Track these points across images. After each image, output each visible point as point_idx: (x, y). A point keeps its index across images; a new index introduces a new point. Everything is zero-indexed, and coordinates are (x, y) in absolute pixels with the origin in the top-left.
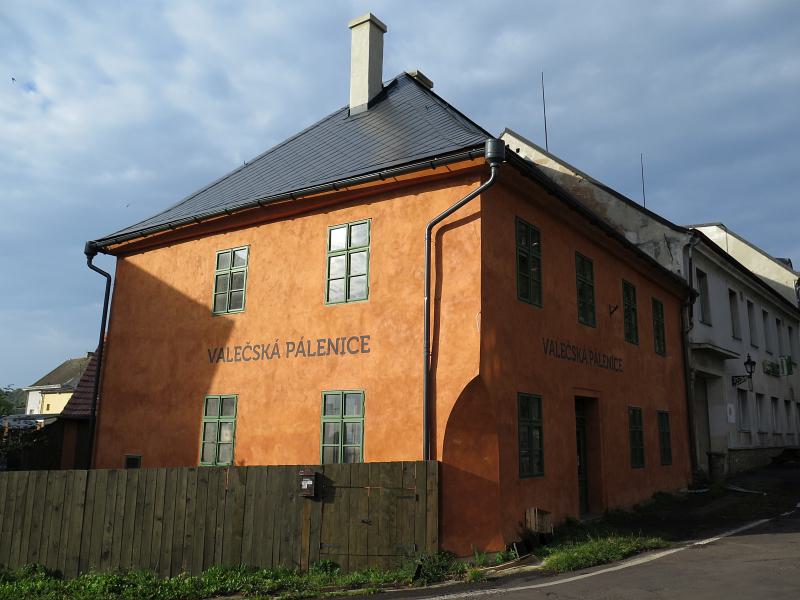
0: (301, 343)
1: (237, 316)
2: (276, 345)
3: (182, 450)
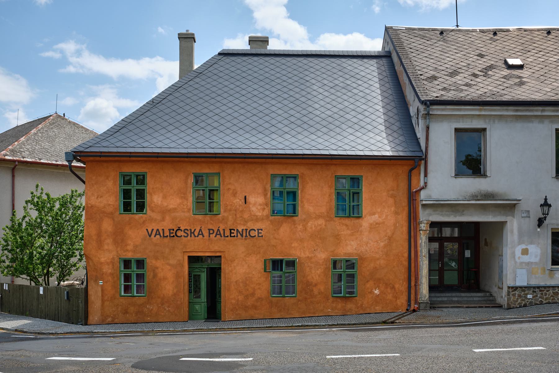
0: (218, 230)
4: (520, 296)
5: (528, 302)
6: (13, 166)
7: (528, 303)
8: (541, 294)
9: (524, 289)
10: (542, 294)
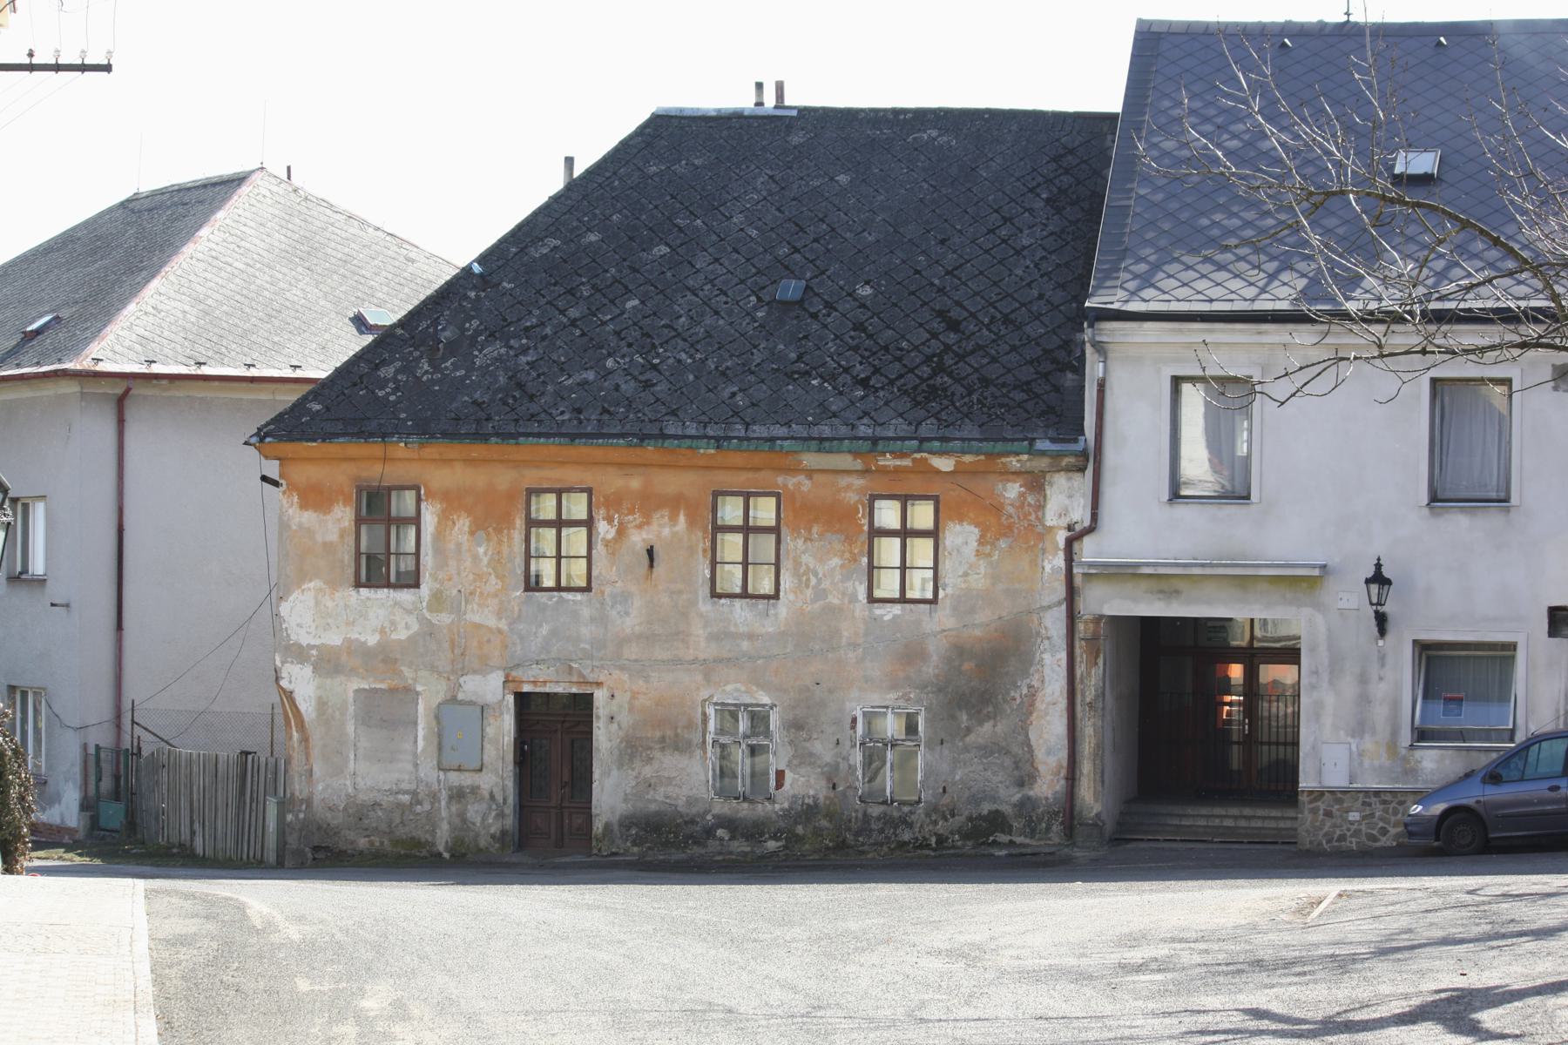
4: (1328, 814)
5: (1349, 830)
6: (119, 391)
7: (1348, 834)
8: (1383, 810)
9: (1339, 795)
10: (1386, 811)
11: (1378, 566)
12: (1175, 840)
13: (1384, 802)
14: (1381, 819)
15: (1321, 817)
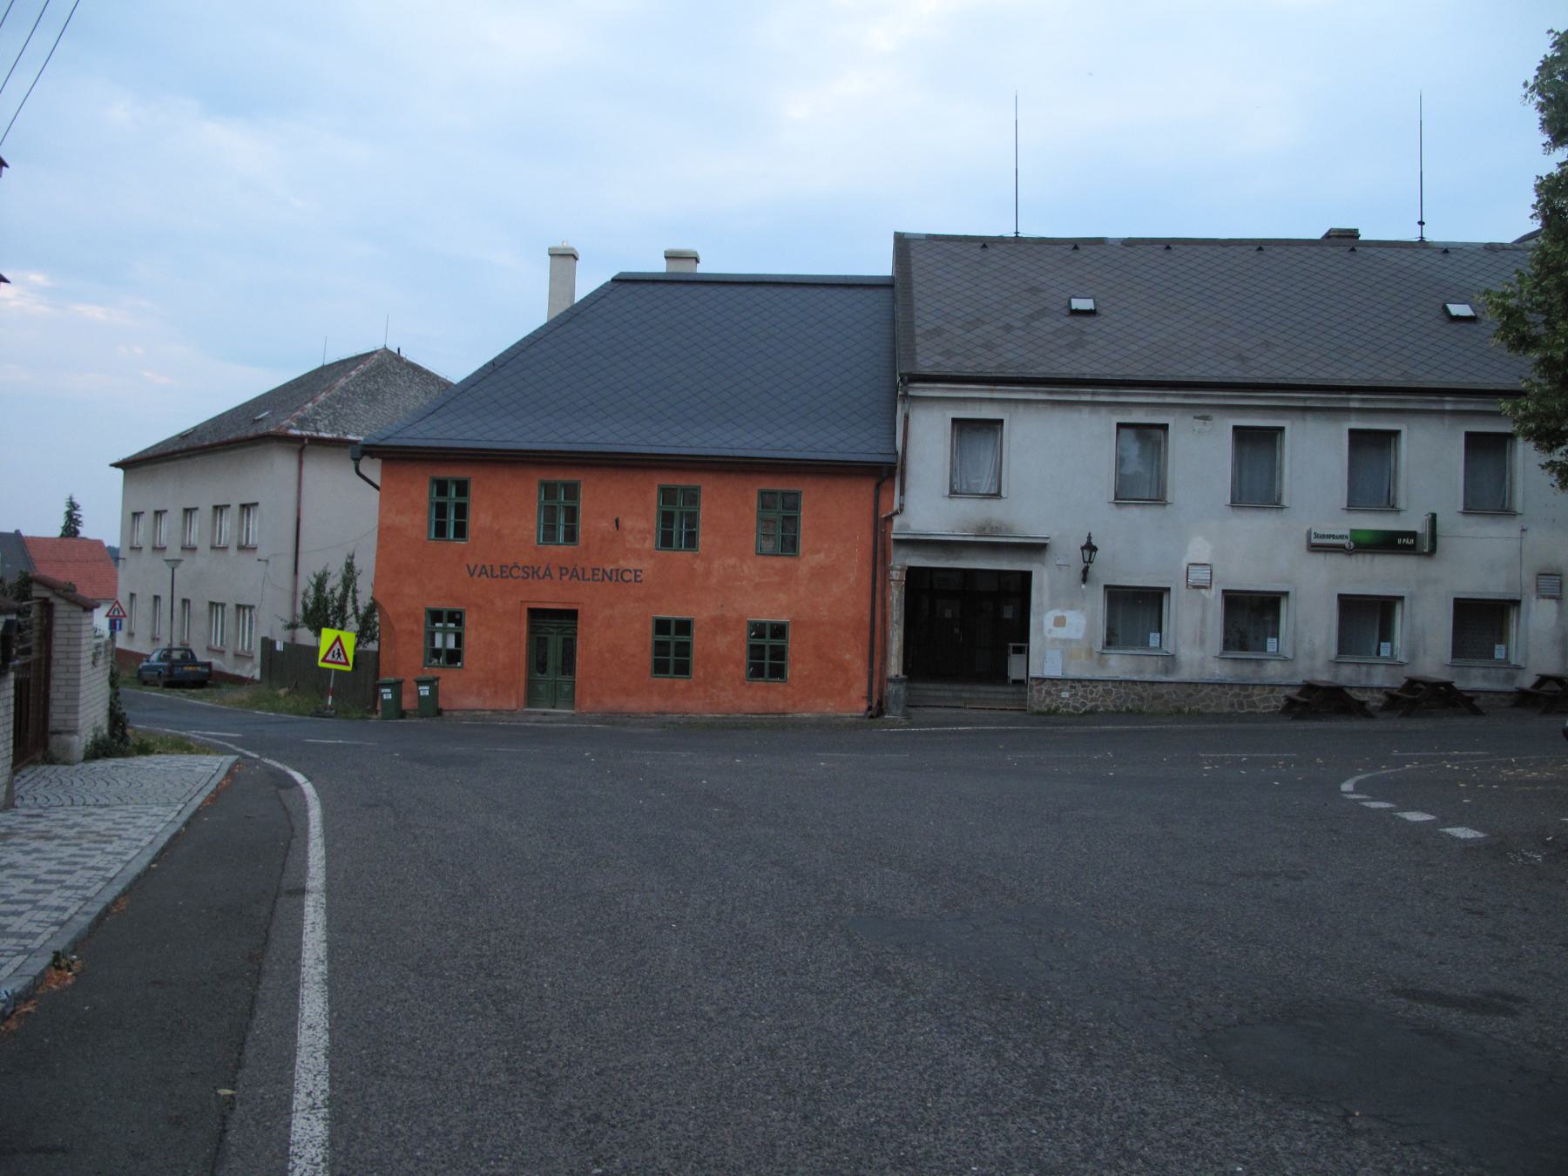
1: (67, 509)
2: (547, 568)
3: (892, 277)
4: (1048, 693)
10: (1085, 692)
11: (1089, 538)
12: (1006, 709)
13: (1084, 686)
14: (1082, 696)
15: (1044, 695)
